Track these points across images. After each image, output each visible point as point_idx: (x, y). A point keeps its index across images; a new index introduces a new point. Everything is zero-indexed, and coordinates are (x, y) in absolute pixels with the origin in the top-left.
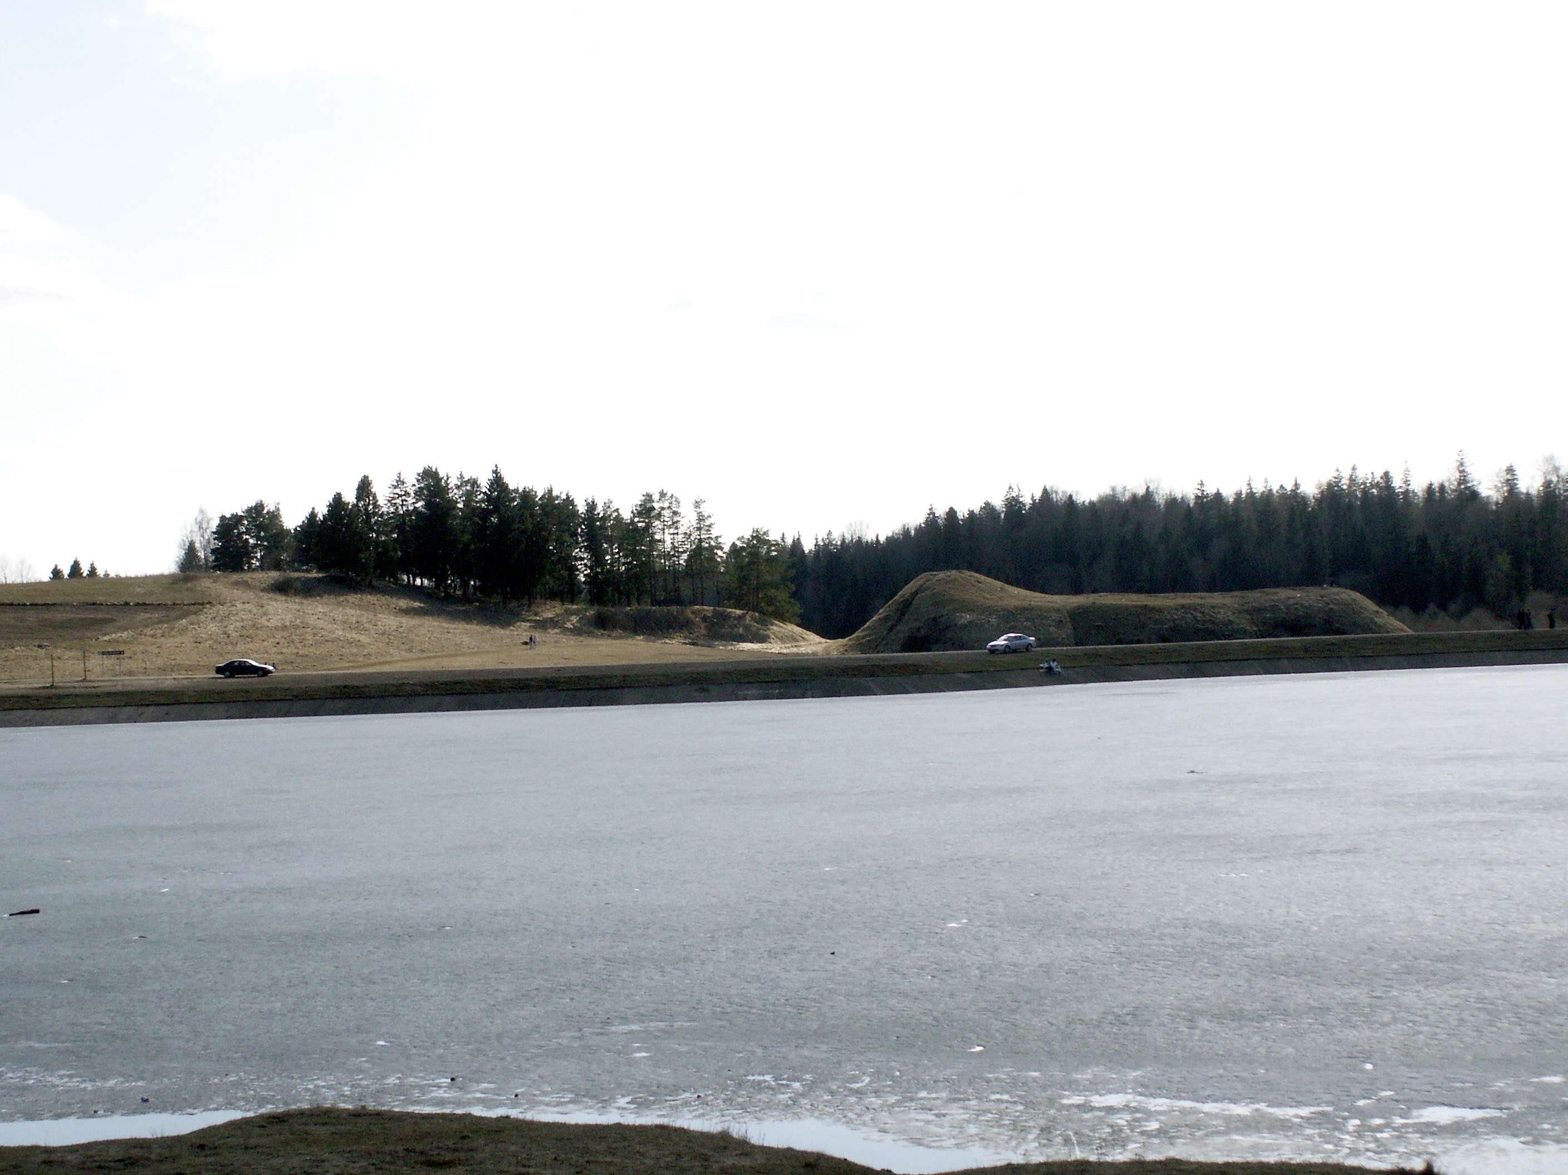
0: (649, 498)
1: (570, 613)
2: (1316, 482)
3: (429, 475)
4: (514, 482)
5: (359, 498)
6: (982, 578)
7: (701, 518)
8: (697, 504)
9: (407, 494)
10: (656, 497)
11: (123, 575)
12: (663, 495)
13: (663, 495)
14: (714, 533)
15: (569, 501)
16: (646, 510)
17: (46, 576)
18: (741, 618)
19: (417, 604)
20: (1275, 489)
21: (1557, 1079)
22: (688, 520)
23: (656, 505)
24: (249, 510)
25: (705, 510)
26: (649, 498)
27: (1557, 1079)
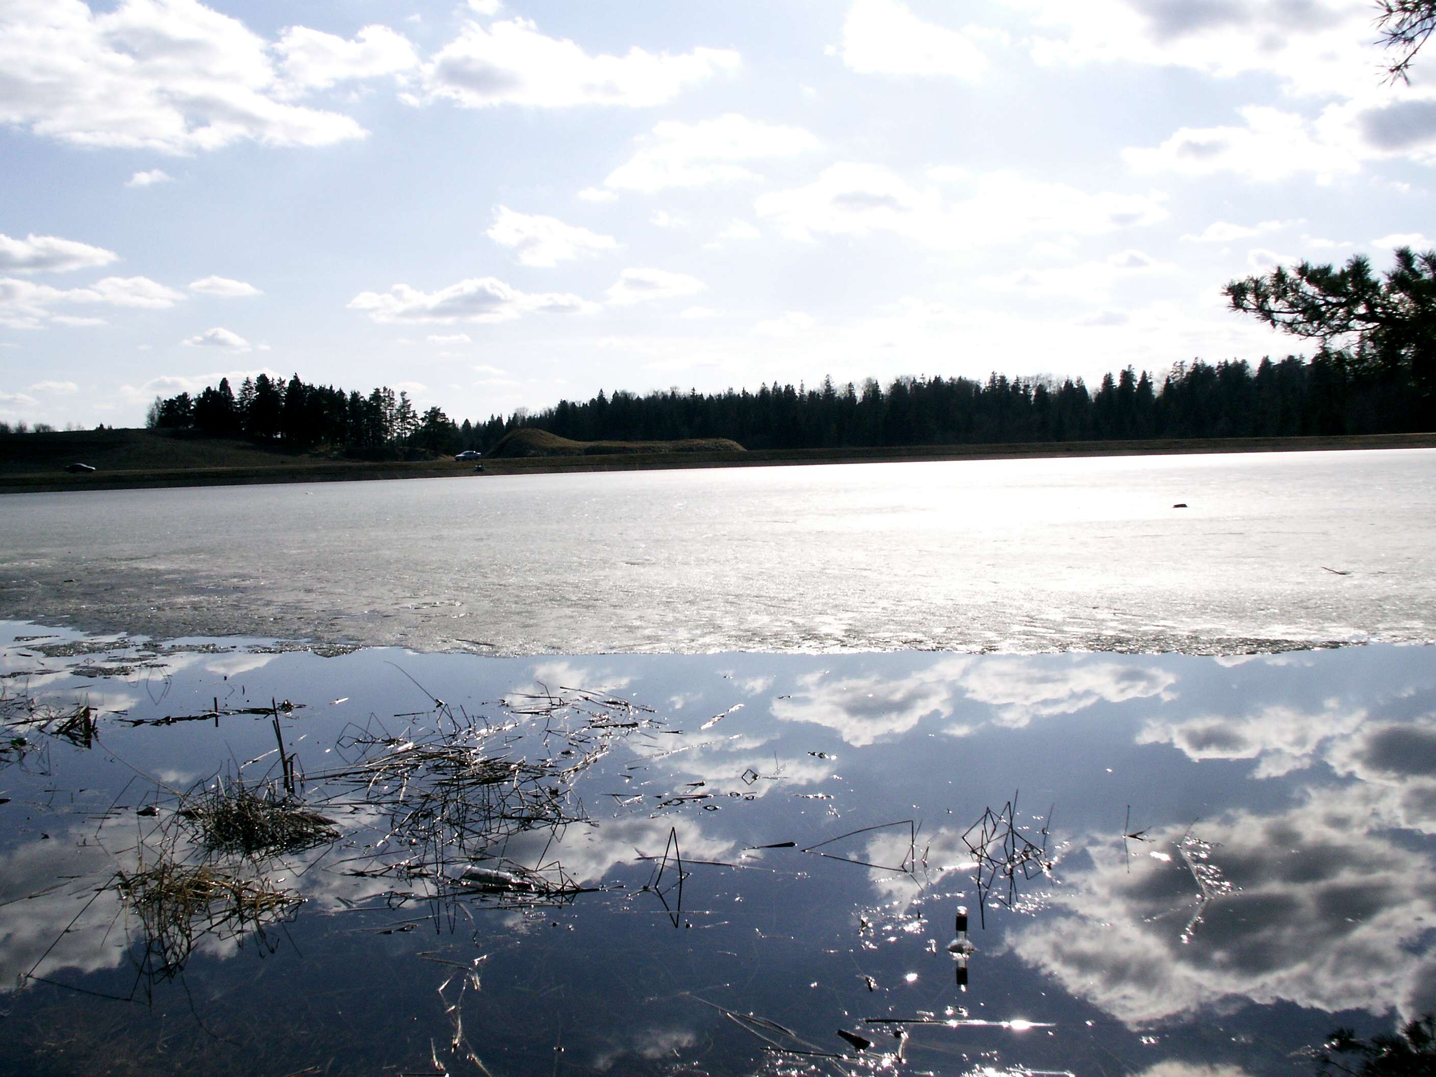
0: (377, 390)
1: (333, 450)
2: (673, 384)
3: (263, 379)
4: (305, 380)
5: (221, 389)
6: (543, 432)
7: (405, 401)
8: (403, 394)
9: (252, 388)
10: (382, 390)
11: (59, 426)
12: (385, 389)
13: (385, 389)
14: (412, 409)
15: (341, 393)
16: (376, 396)
17: (460, 424)
18: (424, 452)
19: (248, 444)
20: (770, 388)
21: (453, 1007)
22: (398, 402)
23: (382, 395)
24: (179, 397)
25: (407, 397)
26: (377, 390)
27: (453, 1007)
